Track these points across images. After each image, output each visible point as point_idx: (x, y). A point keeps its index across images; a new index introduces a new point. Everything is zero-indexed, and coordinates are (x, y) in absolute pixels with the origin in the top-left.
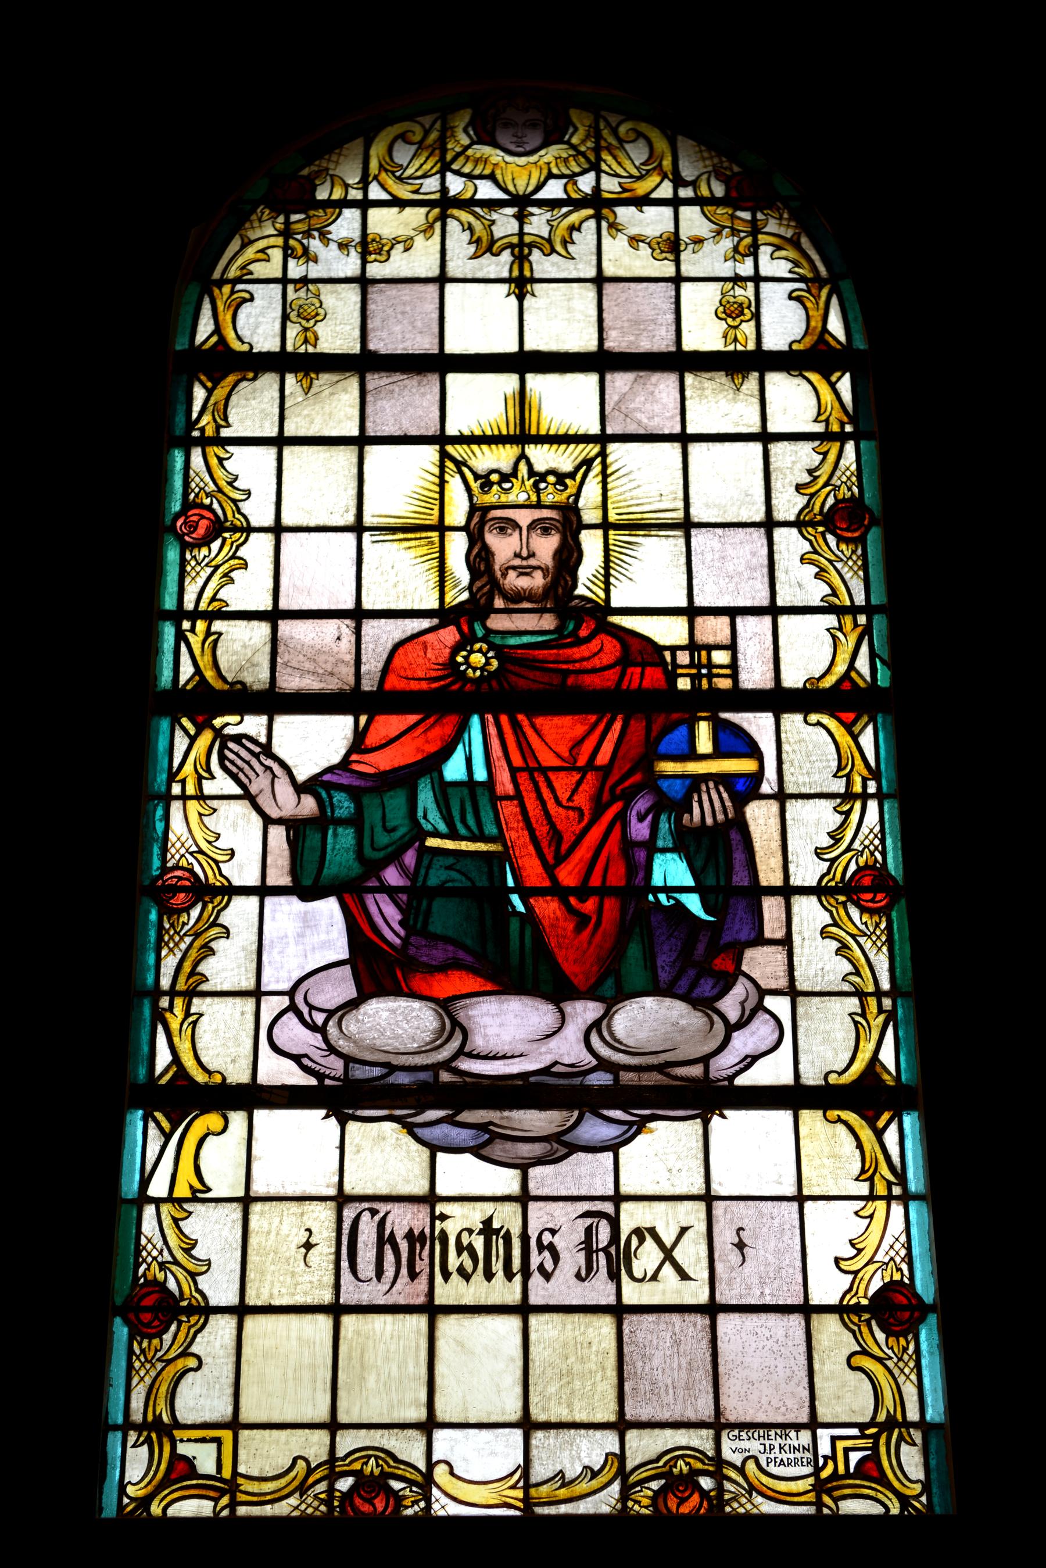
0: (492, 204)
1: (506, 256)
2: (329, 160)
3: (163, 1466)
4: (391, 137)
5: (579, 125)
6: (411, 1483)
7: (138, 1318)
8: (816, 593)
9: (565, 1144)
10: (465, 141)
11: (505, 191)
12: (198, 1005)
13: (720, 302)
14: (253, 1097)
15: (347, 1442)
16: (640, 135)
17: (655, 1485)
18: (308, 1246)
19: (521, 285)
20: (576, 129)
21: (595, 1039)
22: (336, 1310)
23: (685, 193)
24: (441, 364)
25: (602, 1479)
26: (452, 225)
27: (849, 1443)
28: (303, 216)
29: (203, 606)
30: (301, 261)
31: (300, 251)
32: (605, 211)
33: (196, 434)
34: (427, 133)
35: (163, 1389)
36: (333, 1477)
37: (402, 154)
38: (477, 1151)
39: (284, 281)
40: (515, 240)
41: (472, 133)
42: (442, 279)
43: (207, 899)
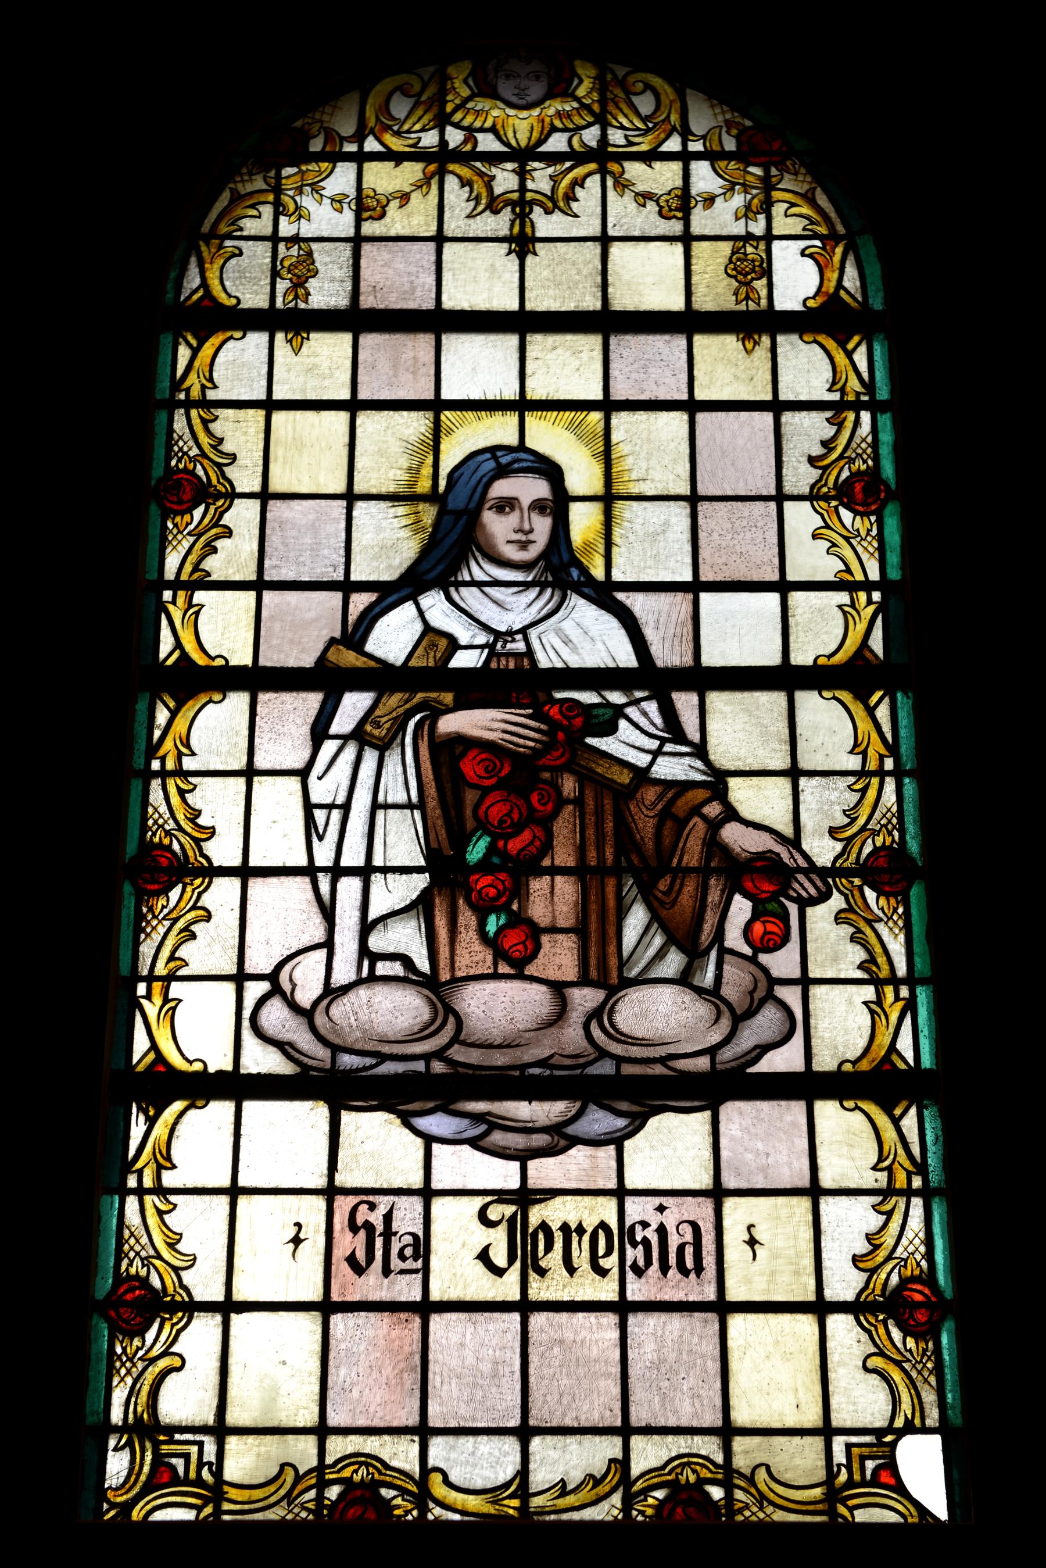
0: (493, 158)
1: (507, 214)
2: (323, 112)
3: (146, 1469)
4: (389, 88)
5: (583, 77)
6: (403, 1492)
7: (118, 1314)
8: (226, 423)
9: (566, 1137)
10: (465, 92)
11: (507, 144)
12: (177, 989)
13: (730, 259)
14: (237, 1086)
15: (338, 1447)
16: (648, 87)
17: (660, 1494)
18: (297, 1241)
19: (522, 244)
20: (581, 81)
21: (596, 1033)
22: (326, 1308)
23: (696, 146)
24: (440, 322)
25: (602, 1489)
26: (451, 183)
27: (865, 1451)
28: (295, 170)
29: (184, 577)
30: (293, 218)
31: (292, 207)
32: (614, 167)
33: (182, 396)
34: (424, 87)
35: (146, 1389)
36: (322, 1485)
37: (400, 108)
38: (474, 1143)
39: (274, 238)
40: (515, 196)
41: (471, 83)
42: (440, 239)
43: (188, 880)
